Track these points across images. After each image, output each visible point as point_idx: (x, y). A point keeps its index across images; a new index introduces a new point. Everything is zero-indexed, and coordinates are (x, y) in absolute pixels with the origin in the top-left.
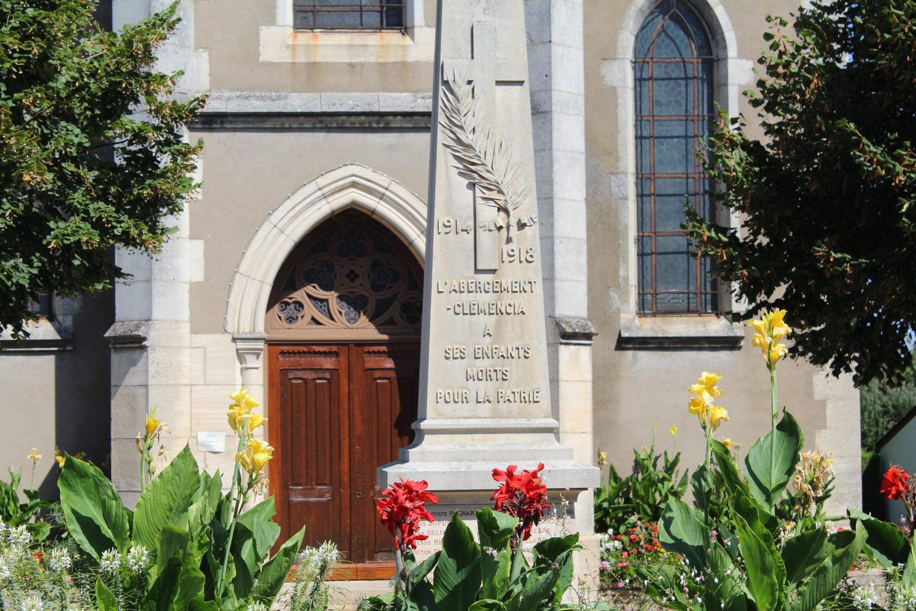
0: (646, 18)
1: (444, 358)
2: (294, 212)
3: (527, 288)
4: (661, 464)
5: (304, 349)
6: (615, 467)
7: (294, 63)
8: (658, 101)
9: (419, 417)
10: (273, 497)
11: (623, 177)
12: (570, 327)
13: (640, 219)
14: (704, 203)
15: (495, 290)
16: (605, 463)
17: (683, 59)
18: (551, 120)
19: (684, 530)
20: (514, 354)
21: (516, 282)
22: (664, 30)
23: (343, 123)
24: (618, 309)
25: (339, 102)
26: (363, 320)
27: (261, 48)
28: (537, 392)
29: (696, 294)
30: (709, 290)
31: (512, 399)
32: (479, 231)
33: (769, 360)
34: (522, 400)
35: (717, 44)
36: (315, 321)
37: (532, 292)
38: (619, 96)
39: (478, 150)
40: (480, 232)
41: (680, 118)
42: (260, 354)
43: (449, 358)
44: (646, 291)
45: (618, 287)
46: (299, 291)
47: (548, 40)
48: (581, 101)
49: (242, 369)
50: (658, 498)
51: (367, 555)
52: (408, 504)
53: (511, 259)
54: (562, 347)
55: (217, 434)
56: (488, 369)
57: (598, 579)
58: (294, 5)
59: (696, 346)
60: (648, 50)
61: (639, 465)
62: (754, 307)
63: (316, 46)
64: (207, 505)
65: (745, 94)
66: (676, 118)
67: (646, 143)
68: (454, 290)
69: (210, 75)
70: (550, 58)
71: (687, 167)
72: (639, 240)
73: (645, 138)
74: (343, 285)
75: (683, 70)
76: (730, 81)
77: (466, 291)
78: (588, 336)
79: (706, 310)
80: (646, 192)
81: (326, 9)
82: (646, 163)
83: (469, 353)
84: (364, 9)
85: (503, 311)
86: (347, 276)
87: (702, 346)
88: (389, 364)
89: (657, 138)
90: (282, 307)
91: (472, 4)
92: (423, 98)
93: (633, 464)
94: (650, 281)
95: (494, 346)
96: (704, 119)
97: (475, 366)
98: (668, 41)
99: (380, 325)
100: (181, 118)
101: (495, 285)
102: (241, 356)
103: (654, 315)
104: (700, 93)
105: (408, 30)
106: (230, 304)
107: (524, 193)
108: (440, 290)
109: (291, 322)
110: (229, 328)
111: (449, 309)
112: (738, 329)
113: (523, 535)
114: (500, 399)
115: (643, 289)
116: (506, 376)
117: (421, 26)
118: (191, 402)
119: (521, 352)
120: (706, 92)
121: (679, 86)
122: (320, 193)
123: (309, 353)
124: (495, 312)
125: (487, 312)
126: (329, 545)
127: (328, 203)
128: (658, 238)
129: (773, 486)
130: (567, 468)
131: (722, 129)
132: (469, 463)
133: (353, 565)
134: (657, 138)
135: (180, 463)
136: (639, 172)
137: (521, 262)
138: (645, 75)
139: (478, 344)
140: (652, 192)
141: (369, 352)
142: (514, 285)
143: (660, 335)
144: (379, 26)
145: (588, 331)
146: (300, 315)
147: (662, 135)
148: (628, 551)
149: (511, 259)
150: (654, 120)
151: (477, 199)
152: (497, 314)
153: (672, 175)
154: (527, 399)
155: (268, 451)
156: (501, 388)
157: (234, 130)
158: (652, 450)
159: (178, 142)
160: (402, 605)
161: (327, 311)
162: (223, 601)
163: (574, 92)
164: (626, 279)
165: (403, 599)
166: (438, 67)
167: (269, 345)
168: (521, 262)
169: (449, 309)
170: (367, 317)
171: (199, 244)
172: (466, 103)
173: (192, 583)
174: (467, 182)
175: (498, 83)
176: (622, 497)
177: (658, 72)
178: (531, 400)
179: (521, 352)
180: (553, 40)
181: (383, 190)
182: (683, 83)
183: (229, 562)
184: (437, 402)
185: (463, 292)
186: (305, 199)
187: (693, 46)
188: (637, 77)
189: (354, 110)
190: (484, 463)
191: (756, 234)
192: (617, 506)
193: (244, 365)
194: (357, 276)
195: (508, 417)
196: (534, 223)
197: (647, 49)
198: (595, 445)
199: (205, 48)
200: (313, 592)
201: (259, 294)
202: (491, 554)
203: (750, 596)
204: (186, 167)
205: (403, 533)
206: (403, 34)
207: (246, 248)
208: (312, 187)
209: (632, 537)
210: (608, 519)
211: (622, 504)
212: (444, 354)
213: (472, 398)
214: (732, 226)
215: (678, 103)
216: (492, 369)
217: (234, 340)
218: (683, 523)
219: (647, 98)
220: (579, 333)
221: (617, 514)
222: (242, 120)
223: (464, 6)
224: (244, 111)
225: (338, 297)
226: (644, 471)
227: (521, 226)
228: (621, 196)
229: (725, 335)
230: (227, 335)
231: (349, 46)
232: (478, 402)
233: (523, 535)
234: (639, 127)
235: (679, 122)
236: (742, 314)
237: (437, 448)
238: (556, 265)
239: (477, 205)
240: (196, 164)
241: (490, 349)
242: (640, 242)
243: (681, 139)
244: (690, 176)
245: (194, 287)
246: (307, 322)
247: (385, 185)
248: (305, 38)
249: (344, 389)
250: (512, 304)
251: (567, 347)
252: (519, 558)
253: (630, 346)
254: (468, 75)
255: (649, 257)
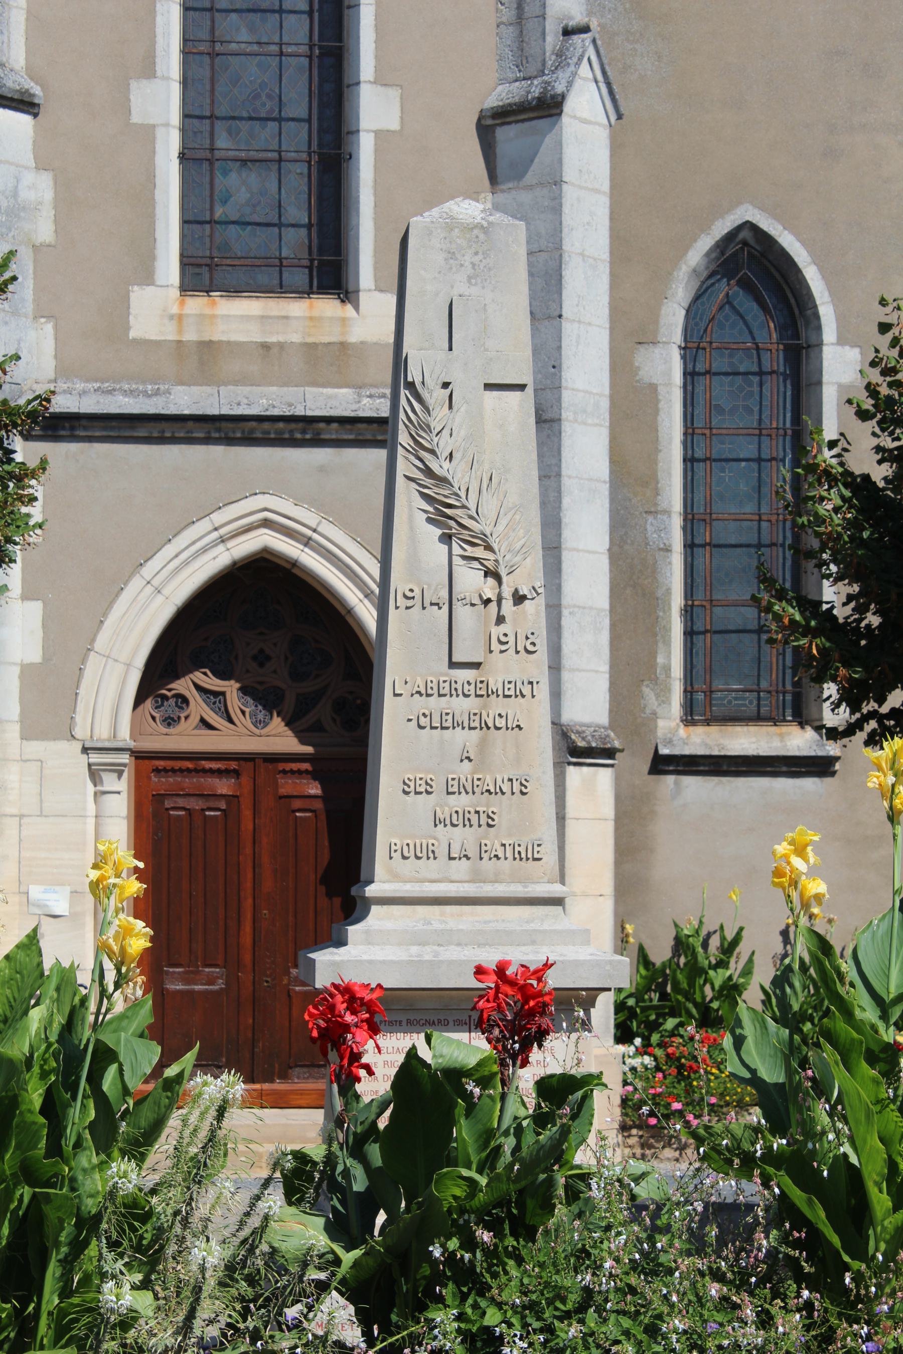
0: (703, 282)
1: (401, 792)
2: (177, 562)
3: (526, 690)
4: (715, 942)
5: (189, 765)
6: (645, 946)
7: (179, 342)
8: (718, 407)
9: (363, 878)
10: (149, 996)
11: (665, 517)
12: (583, 739)
13: (689, 581)
14: (784, 558)
15: (479, 692)
16: (631, 940)
17: (756, 344)
18: (560, 433)
19: (758, 1053)
20: (506, 788)
21: (510, 682)
22: (728, 301)
23: (252, 431)
24: (654, 713)
25: (246, 401)
26: (277, 724)
27: (131, 318)
28: (539, 845)
29: (769, 692)
30: (789, 687)
31: (501, 855)
32: (457, 606)
33: (891, 808)
34: (517, 856)
35: (807, 323)
36: (205, 724)
37: (533, 696)
38: (660, 397)
39: (456, 486)
40: (457, 607)
41: (751, 432)
42: (123, 771)
43: (409, 793)
44: (696, 687)
45: (655, 680)
46: (183, 679)
47: (557, 313)
48: (605, 404)
49: (95, 794)
50: (708, 992)
51: (277, 1070)
52: (349, 1018)
53: (503, 648)
54: (571, 768)
55: (57, 888)
56: (467, 809)
57: (618, 1111)
58: (182, 256)
59: (769, 769)
60: (705, 331)
61: (680, 945)
62: (858, 719)
63: (213, 317)
64: (55, 1011)
65: (849, 402)
66: (745, 431)
67: (700, 467)
68: (419, 692)
69: (56, 357)
70: (560, 341)
71: (759, 504)
72: (686, 611)
73: (699, 460)
74: (248, 671)
75: (755, 360)
76: (825, 378)
77: (436, 695)
78: (610, 753)
79: (784, 716)
80: (697, 541)
81: (229, 262)
82: (699, 497)
83: (438, 786)
84: (285, 262)
85: (490, 724)
86: (255, 658)
87: (778, 769)
88: (314, 789)
89: (715, 460)
90: (157, 702)
91: (451, 268)
92: (370, 396)
93: (673, 943)
94: (702, 673)
95: (476, 777)
96: (785, 434)
97: (448, 806)
98: (734, 317)
99: (302, 731)
100: (15, 425)
101: (479, 685)
102: (94, 774)
103: (708, 722)
104: (781, 394)
105: (349, 295)
106: (79, 698)
107: (524, 550)
108: (397, 692)
109: (169, 724)
110: (78, 732)
111: (409, 720)
112: (832, 749)
113: (519, 1063)
114: (483, 855)
115: (692, 685)
116: (493, 820)
117: (370, 290)
118: (20, 840)
119: (516, 785)
120: (789, 393)
121: (750, 384)
122: (215, 535)
123: (196, 771)
124: (478, 725)
125: (466, 725)
126: (231, 1078)
127: (228, 549)
128: (716, 610)
129: (892, 996)
130: (582, 957)
131: (815, 456)
132: (436, 948)
133: (257, 1086)
134: (715, 460)
135: (21, 956)
136: (689, 511)
137: (517, 652)
138: (700, 368)
139: (453, 773)
140: (708, 541)
141: (284, 772)
142: (507, 686)
143: (716, 752)
144: (307, 289)
145: (609, 746)
146: (183, 715)
147: (724, 457)
148: (663, 1072)
149: (503, 648)
150: (712, 435)
151: (454, 557)
152: (481, 728)
153: (737, 517)
154: (523, 855)
155: (145, 935)
156: (485, 838)
157: (90, 439)
158: (701, 922)
159: (10, 461)
160: (337, 1163)
161: (223, 709)
162: (75, 1155)
163: (595, 391)
164: (667, 669)
165: (339, 1153)
166: (399, 362)
167: (137, 758)
168: (517, 652)
169: (409, 720)
170: (283, 720)
171: (36, 608)
172: (439, 416)
173: (28, 1129)
174: (439, 532)
175: (489, 387)
176: (655, 991)
177: (720, 363)
178: (530, 856)
179: (516, 785)
180: (564, 314)
181: (309, 533)
182: (756, 379)
183: (84, 1097)
184: (391, 858)
185: (431, 695)
186: (194, 543)
187: (772, 325)
188: (688, 370)
189: (268, 413)
190: (459, 949)
191: (861, 610)
192: (648, 1004)
193: (99, 788)
194: (268, 658)
195: (496, 881)
196: (538, 594)
197: (703, 328)
198: (616, 913)
199: (49, 317)
200: (206, 1144)
201: (124, 682)
202: (471, 1091)
203: (854, 1159)
204: (20, 498)
205: (342, 1058)
206: (343, 301)
207: (105, 614)
208: (203, 526)
209: (670, 1050)
210: (635, 1024)
211: (655, 1002)
212: (402, 786)
213: (442, 852)
214: (825, 599)
215: (750, 411)
216: (472, 811)
217: (85, 750)
218: (756, 1044)
219: (702, 402)
220: (596, 748)
221: (648, 1017)
222: (102, 424)
223: (440, 272)
224: (105, 412)
225: (240, 689)
226: (689, 954)
227: (519, 599)
228: (662, 546)
229: (813, 754)
230: (74, 742)
231: (262, 317)
232: (451, 858)
233: (519, 1063)
234: (689, 445)
235: (748, 438)
236: (841, 729)
237: (389, 925)
238: (564, 646)
239: (454, 567)
240: (36, 494)
241: (470, 780)
242: (689, 614)
243: (751, 463)
244: (764, 517)
245: (27, 671)
246: (195, 724)
247: (313, 525)
248: (196, 304)
249: (247, 825)
250: (504, 714)
251: (577, 768)
252: (511, 1100)
253: (671, 768)
254: (444, 373)
255: (701, 637)
